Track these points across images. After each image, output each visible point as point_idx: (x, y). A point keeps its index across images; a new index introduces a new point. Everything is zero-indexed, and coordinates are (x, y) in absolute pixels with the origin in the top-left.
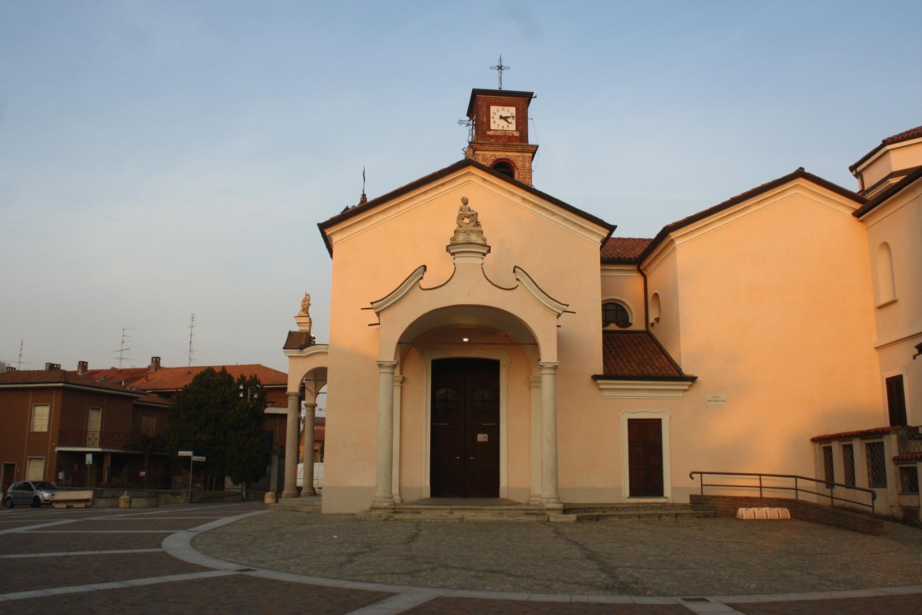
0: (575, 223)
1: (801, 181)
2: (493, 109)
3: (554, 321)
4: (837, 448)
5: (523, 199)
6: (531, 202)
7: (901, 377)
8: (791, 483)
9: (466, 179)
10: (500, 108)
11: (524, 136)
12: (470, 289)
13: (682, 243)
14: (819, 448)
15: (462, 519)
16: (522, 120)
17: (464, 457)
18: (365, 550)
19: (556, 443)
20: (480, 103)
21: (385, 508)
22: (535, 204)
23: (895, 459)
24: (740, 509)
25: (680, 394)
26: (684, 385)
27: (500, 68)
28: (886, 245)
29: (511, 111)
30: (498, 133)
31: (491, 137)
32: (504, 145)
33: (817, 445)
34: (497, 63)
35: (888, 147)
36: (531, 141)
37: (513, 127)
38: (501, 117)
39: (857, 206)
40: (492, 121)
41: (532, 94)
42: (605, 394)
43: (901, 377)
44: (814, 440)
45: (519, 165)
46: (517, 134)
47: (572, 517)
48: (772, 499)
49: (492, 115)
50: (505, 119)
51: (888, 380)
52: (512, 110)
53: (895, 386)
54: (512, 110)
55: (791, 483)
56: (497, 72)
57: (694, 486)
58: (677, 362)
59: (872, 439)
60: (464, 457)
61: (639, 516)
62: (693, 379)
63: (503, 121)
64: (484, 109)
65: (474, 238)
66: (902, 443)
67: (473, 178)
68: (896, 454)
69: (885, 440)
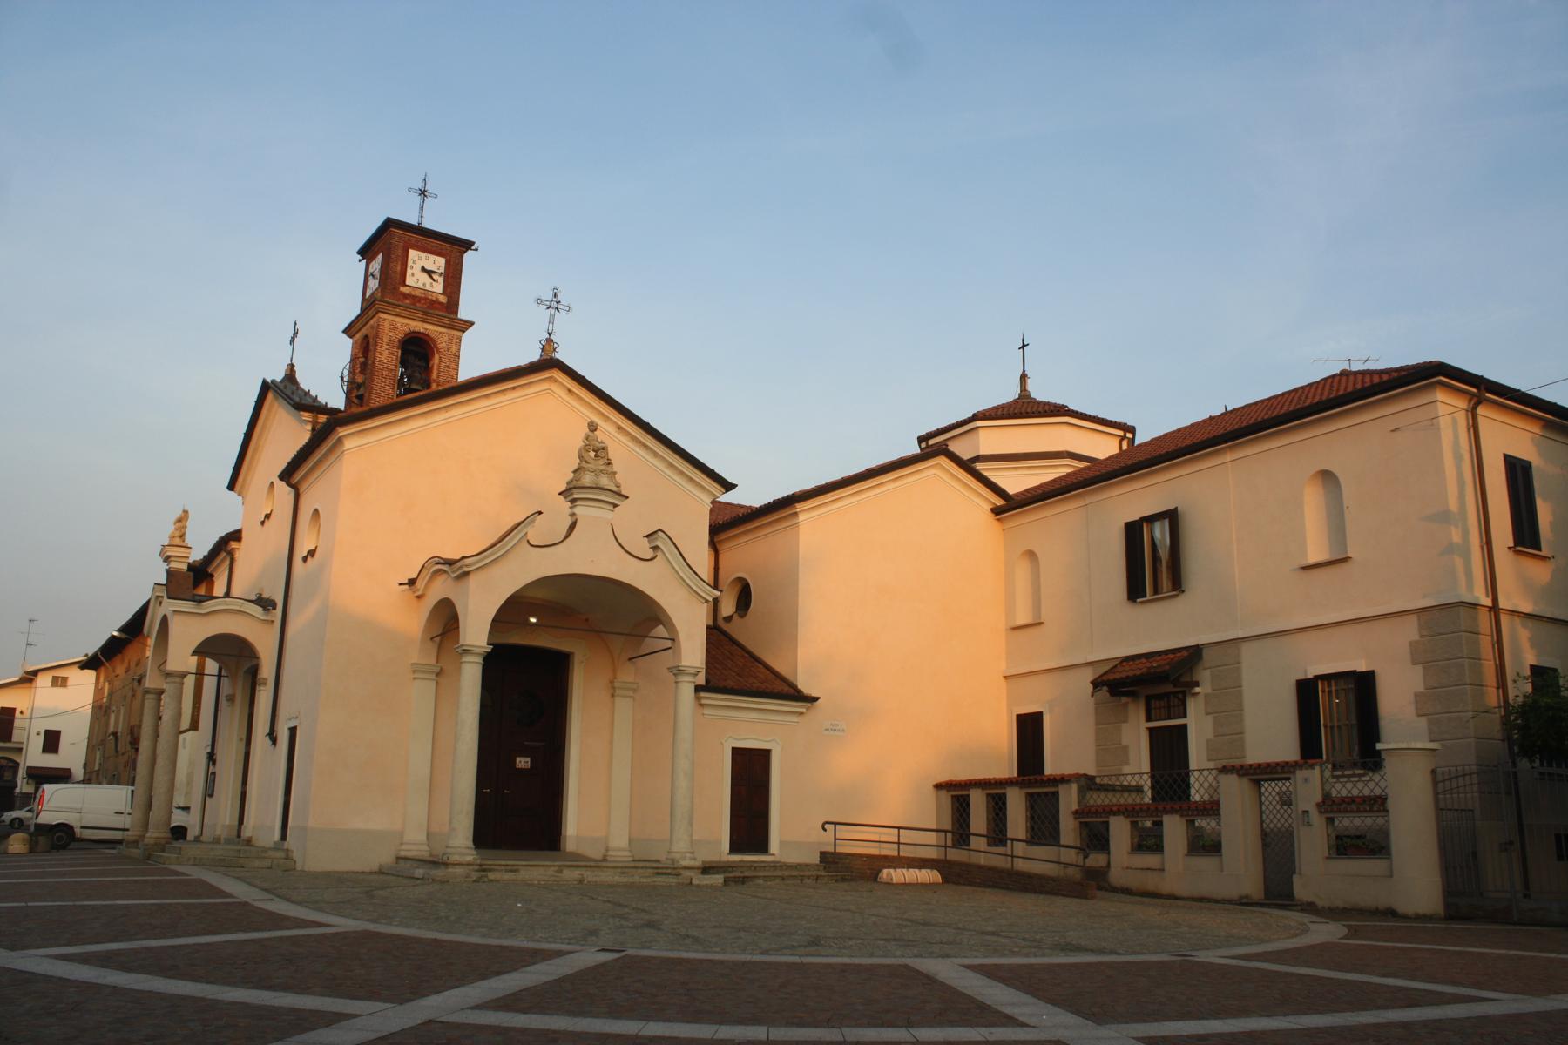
0: (682, 473)
1: (942, 460)
2: (413, 254)
3: (165, 566)
4: (978, 800)
5: (619, 428)
6: (629, 434)
7: (1040, 714)
8: (892, 835)
9: (545, 386)
10: (423, 255)
11: (453, 304)
12: (591, 555)
13: (806, 515)
14: (946, 797)
15: (581, 881)
16: (453, 278)
17: (519, 794)
18: (853, 908)
19: (639, 777)
20: (388, 243)
21: (469, 864)
22: (634, 439)
23: (1076, 813)
24: (885, 871)
25: (795, 718)
26: (799, 707)
27: (423, 192)
28: (1031, 555)
29: (438, 263)
30: (416, 293)
31: (406, 296)
32: (425, 313)
33: (943, 793)
34: (419, 185)
35: (979, 423)
36: (463, 314)
37: (438, 287)
38: (423, 269)
39: (999, 502)
40: (409, 272)
41: (472, 243)
42: (707, 711)
43: (1040, 714)
44: (938, 787)
45: (442, 346)
46: (443, 299)
47: (718, 879)
48: (913, 859)
49: (410, 263)
50: (430, 273)
51: (1019, 716)
52: (441, 261)
53: (1029, 728)
54: (441, 261)
55: (892, 835)
56: (418, 199)
57: (826, 840)
58: (791, 679)
59: (995, 790)
60: (519, 794)
61: (783, 879)
62: (816, 699)
63: (425, 275)
64: (400, 252)
65: (604, 481)
66: (1082, 792)
67: (554, 387)
68: (1075, 807)
69: (1062, 789)
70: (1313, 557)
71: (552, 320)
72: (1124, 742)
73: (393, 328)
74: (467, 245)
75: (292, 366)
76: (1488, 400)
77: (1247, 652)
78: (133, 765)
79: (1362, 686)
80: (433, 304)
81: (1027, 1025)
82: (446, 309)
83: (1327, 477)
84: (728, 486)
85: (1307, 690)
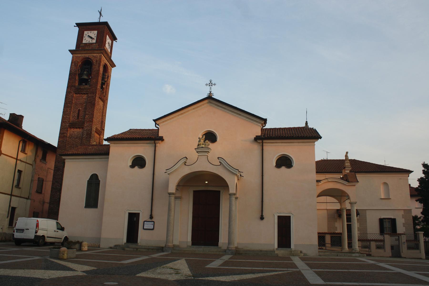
17: (206, 227)
22: (178, 115)
41: (117, 39)
60: (206, 227)
70: (382, 197)
71: (211, 89)
72: (336, 226)
75: (307, 122)
76: (265, 142)
77: (367, 212)
78: (323, 236)
79: (393, 221)
83: (385, 184)
85: (381, 221)
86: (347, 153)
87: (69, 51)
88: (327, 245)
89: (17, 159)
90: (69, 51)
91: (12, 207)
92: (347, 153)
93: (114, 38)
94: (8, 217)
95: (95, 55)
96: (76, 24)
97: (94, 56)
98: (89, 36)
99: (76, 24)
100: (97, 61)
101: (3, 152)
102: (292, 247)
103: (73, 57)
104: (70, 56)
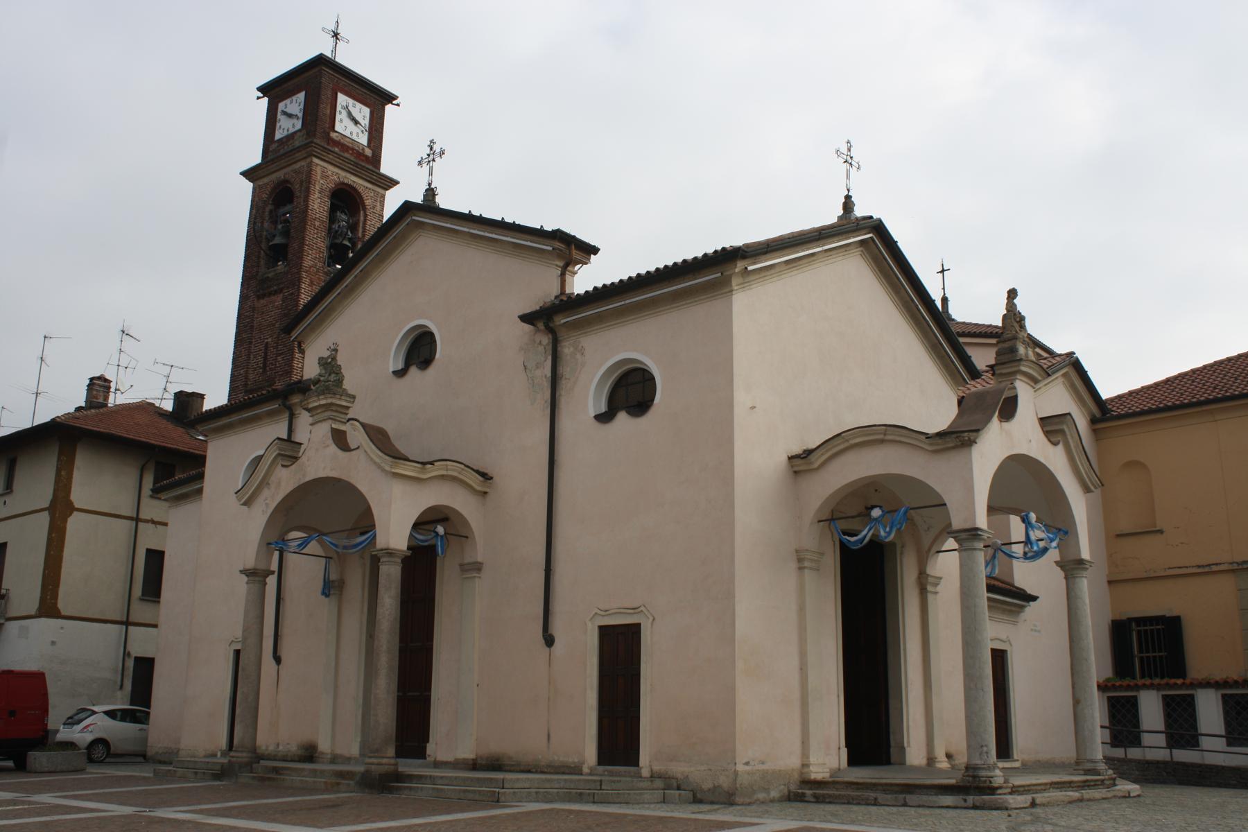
11: (376, 160)
16: (376, 130)
37: (363, 139)
41: (395, 98)
64: (329, 93)
73: (325, 177)
74: (389, 98)
75: (848, 198)
80: (359, 154)
81: (478, 472)
82: (367, 161)
84: (572, 250)
86: (1012, 294)
87: (397, 183)
88: (1147, 739)
89: (137, 520)
90: (397, 183)
91: (137, 659)
92: (1012, 294)
93: (377, 98)
94: (121, 687)
95: (297, 166)
96: (259, 89)
97: (295, 171)
98: (356, 122)
99: (259, 89)
100: (302, 182)
101: (77, 506)
102: (641, 764)
103: (254, 189)
104: (248, 186)
